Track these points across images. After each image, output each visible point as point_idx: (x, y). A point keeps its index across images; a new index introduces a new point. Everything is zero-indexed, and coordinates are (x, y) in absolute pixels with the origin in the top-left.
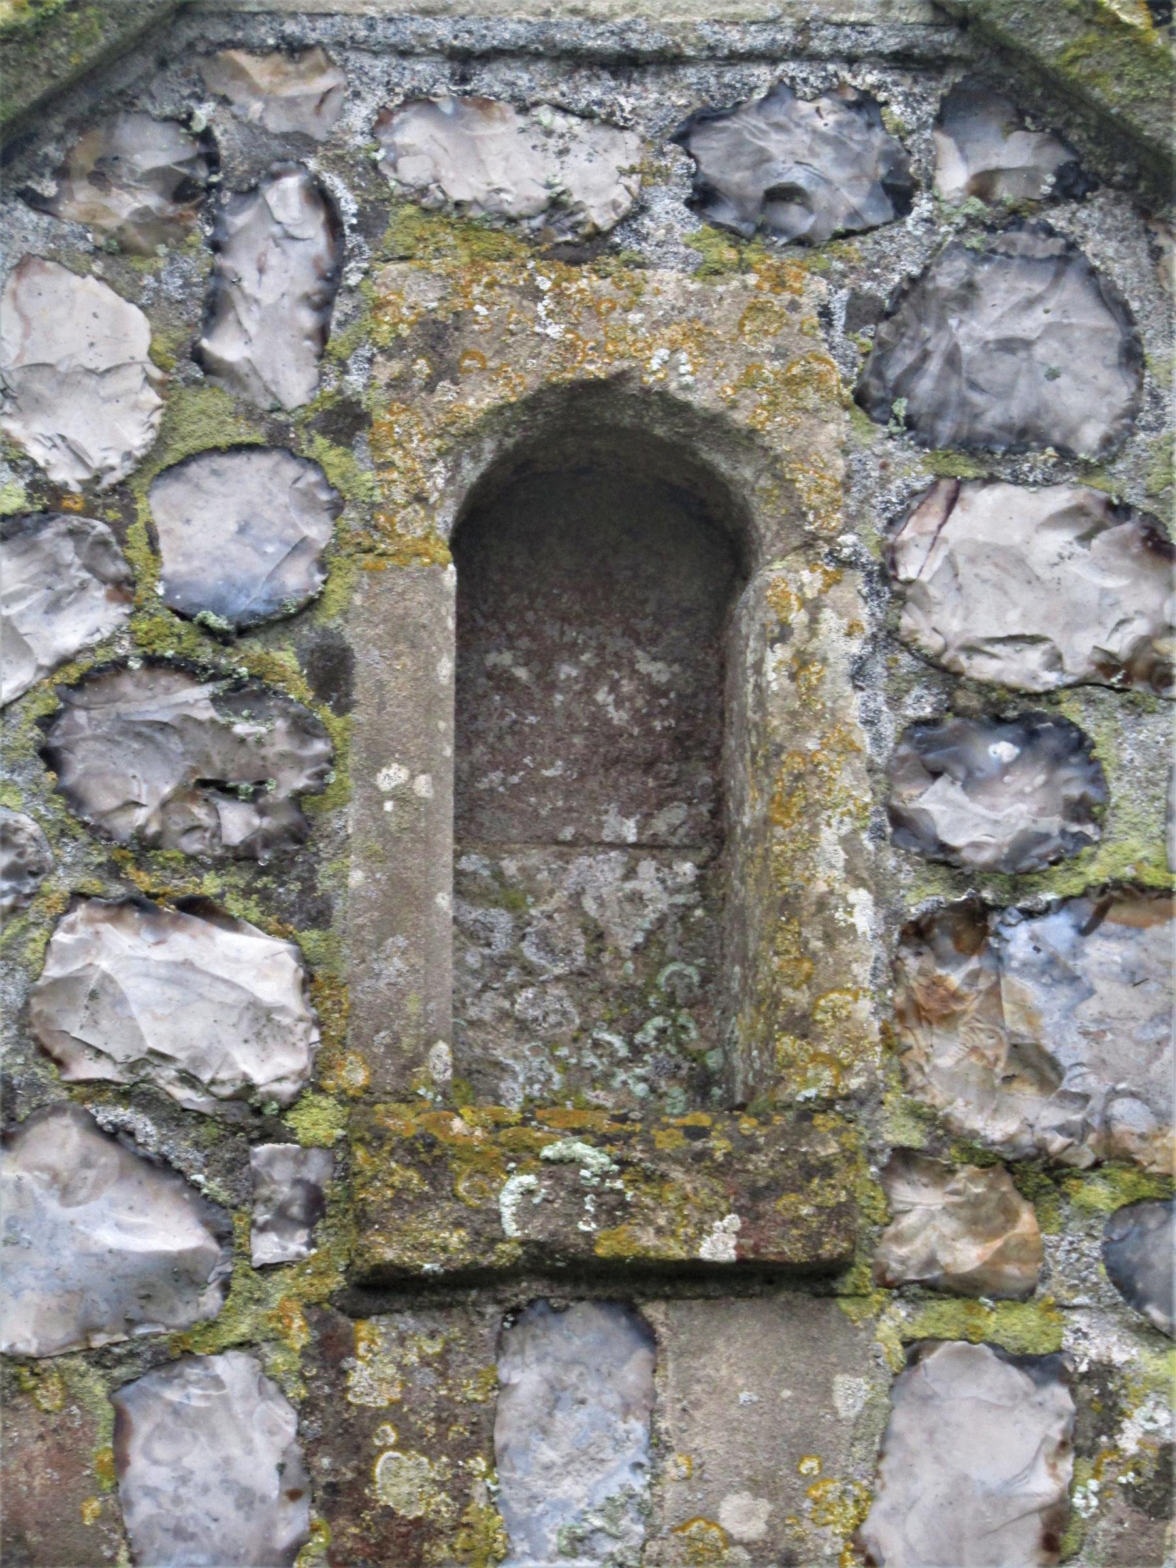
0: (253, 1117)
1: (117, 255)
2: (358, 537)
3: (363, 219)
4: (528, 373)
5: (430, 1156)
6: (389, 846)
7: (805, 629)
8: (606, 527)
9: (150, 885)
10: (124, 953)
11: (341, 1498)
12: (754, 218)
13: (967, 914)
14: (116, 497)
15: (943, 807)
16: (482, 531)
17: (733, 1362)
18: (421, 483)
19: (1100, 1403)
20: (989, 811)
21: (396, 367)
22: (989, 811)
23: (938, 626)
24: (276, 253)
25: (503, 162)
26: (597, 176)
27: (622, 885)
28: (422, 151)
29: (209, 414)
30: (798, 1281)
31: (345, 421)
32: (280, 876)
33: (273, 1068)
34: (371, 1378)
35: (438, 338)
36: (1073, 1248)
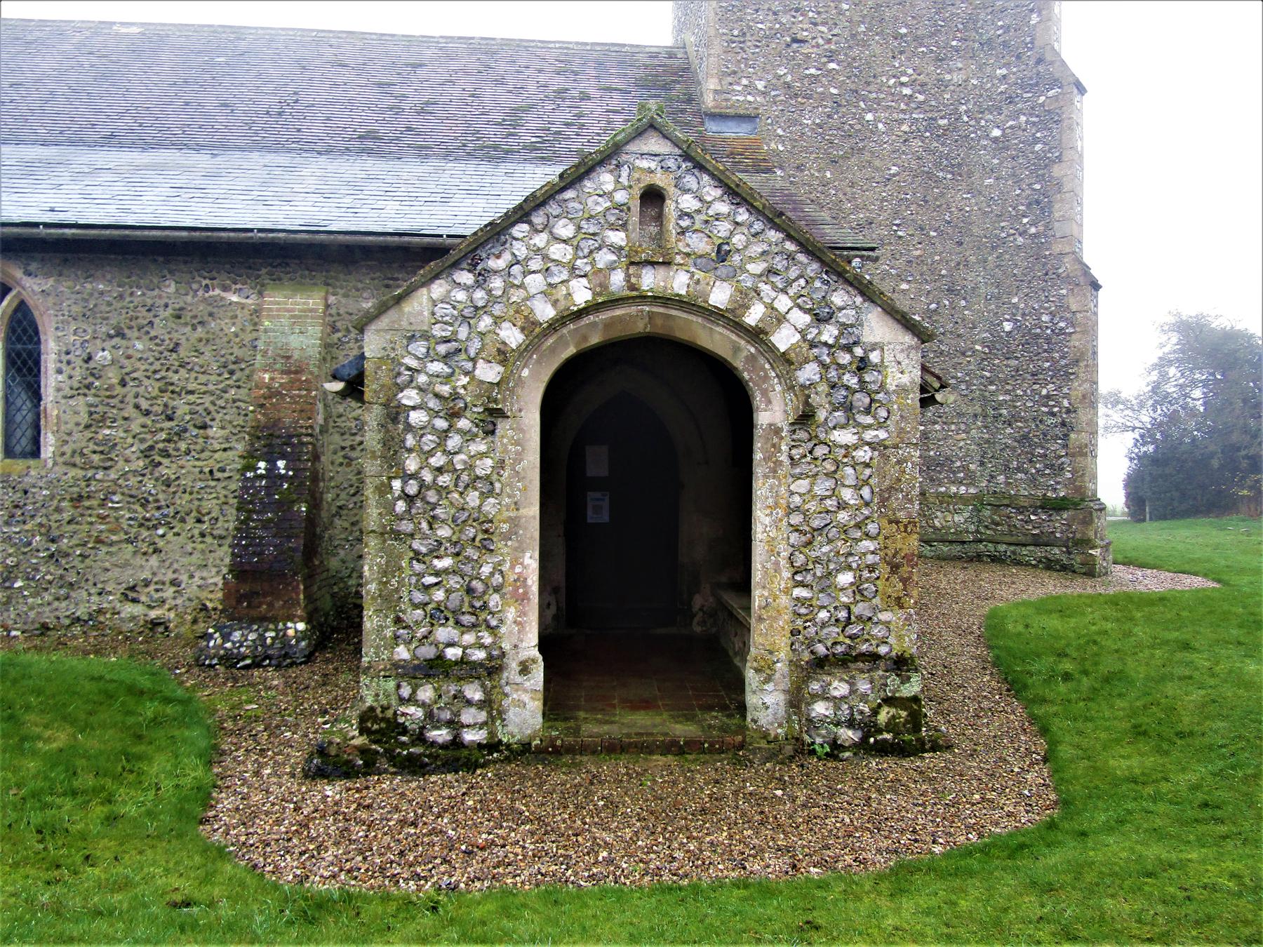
0: (621, 248)
1: (611, 171)
2: (631, 197)
3: (632, 169)
4: (647, 183)
5: (636, 252)
6: (634, 225)
7: (670, 208)
8: (653, 197)
9: (613, 227)
10: (610, 233)
11: (628, 281)
12: (667, 170)
13: (683, 232)
14: (611, 193)
15: (681, 222)
16: (642, 197)
17: (661, 271)
18: (637, 192)
19: (693, 275)
20: (685, 223)
21: (175, 523)
22: (685, 223)
23: (681, 206)
24: (625, 172)
25: (644, 164)
26: (653, 165)
27: (653, 229)
28: (639, 163)
29: (619, 186)
30: (667, 264)
31: (630, 187)
32: (624, 227)
33: (623, 244)
34: (631, 271)
35: (639, 180)
36: (691, 261)
